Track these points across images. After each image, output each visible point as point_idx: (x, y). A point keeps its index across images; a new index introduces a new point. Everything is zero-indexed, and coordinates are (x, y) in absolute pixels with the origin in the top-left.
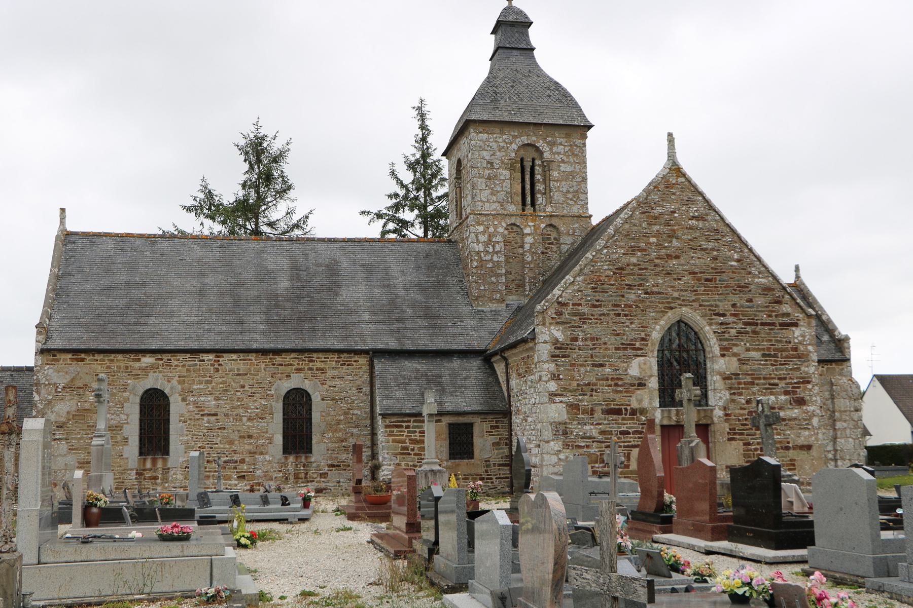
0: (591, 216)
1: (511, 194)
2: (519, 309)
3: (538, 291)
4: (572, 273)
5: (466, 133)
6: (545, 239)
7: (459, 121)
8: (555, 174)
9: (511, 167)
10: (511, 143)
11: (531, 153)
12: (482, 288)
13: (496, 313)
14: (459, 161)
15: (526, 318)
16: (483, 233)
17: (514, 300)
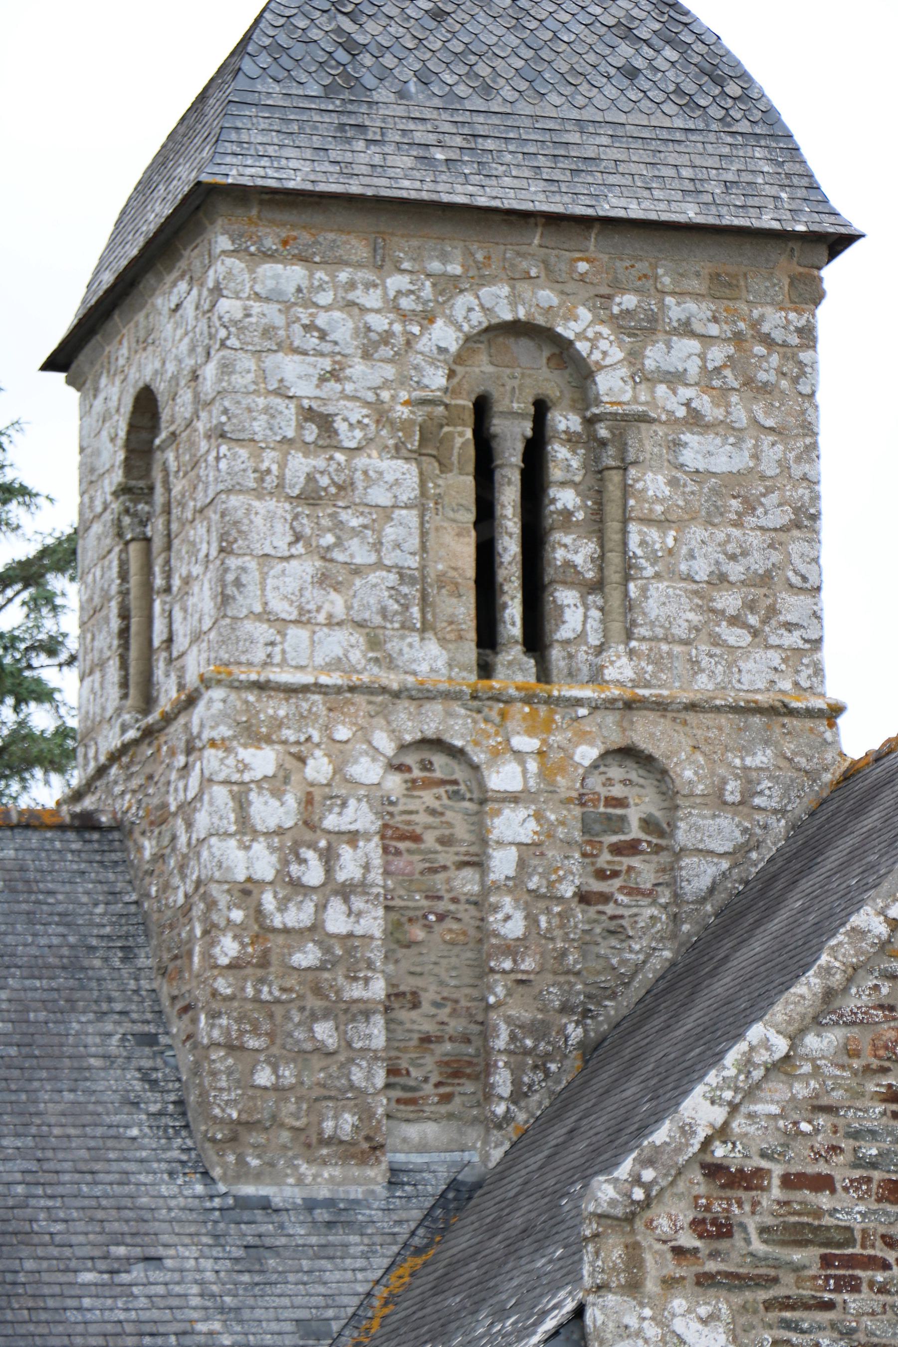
0: (835, 711)
1: (422, 585)
2: (459, 1195)
3: (562, 1104)
4: (779, 1012)
5: (191, 257)
6: (599, 821)
7: (145, 187)
8: (653, 484)
9: (426, 445)
10: (428, 318)
11: (537, 375)
12: (264, 1077)
13: (336, 1215)
14: (146, 405)
15: (512, 1249)
16: (276, 784)
17: (430, 1146)
